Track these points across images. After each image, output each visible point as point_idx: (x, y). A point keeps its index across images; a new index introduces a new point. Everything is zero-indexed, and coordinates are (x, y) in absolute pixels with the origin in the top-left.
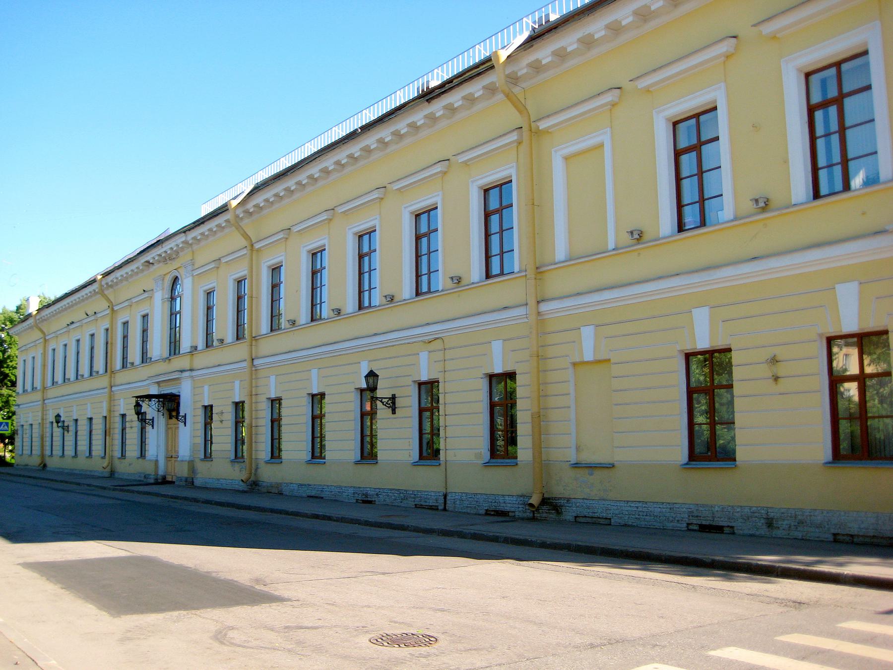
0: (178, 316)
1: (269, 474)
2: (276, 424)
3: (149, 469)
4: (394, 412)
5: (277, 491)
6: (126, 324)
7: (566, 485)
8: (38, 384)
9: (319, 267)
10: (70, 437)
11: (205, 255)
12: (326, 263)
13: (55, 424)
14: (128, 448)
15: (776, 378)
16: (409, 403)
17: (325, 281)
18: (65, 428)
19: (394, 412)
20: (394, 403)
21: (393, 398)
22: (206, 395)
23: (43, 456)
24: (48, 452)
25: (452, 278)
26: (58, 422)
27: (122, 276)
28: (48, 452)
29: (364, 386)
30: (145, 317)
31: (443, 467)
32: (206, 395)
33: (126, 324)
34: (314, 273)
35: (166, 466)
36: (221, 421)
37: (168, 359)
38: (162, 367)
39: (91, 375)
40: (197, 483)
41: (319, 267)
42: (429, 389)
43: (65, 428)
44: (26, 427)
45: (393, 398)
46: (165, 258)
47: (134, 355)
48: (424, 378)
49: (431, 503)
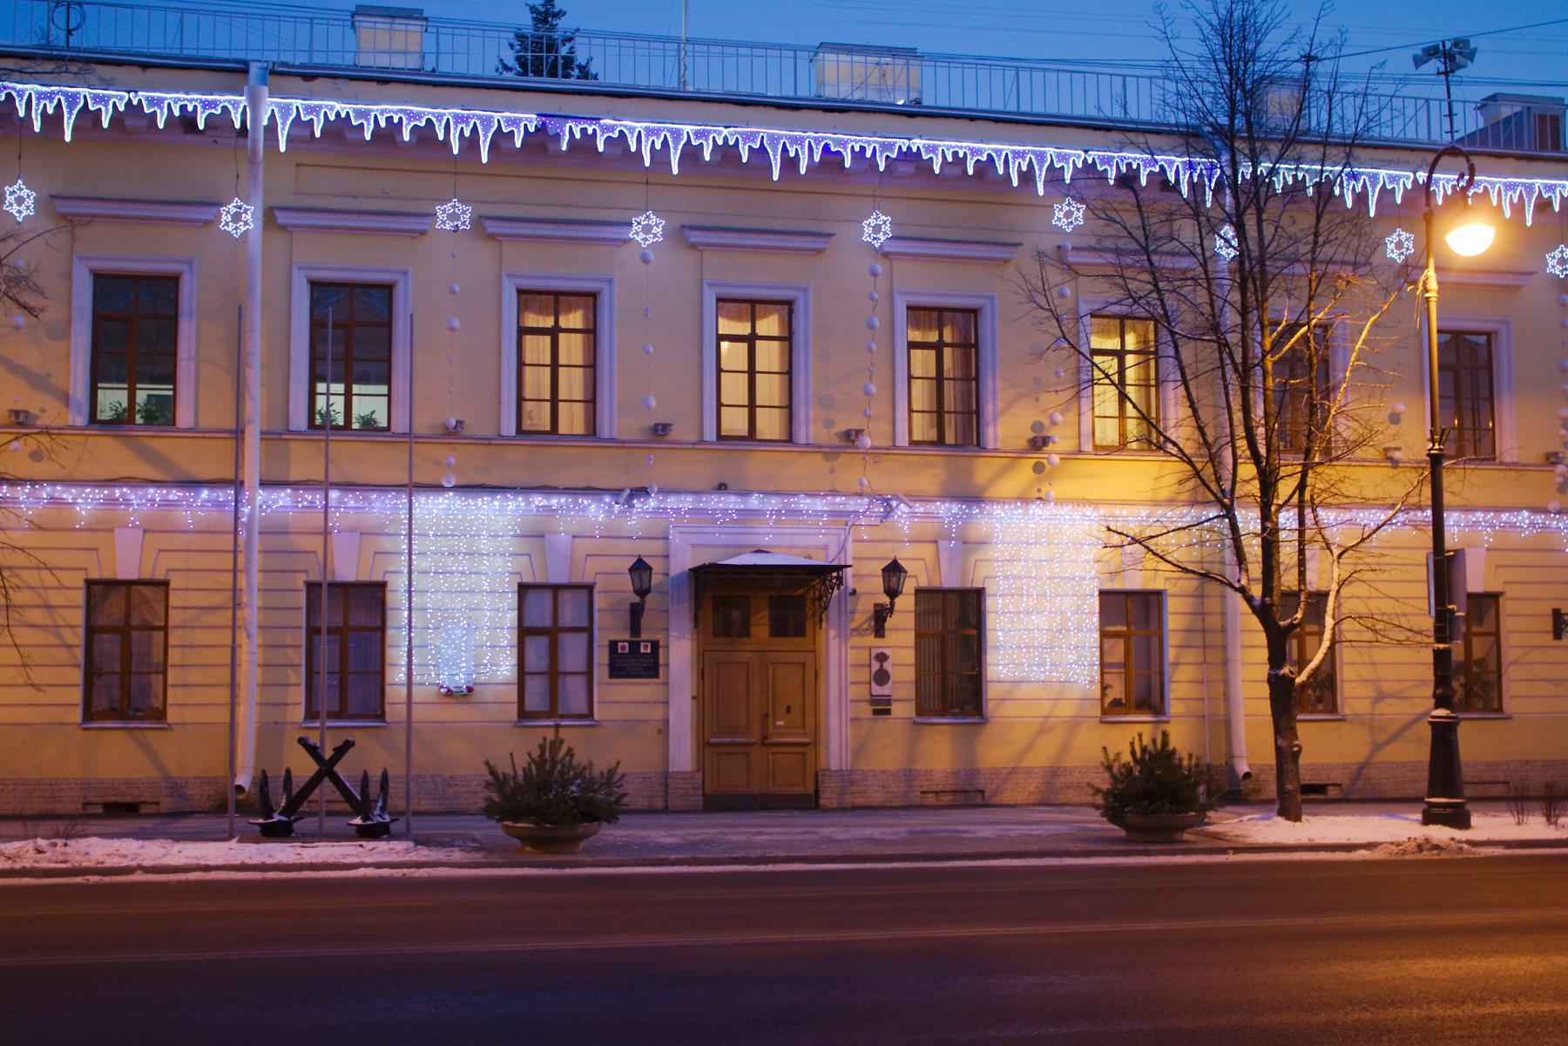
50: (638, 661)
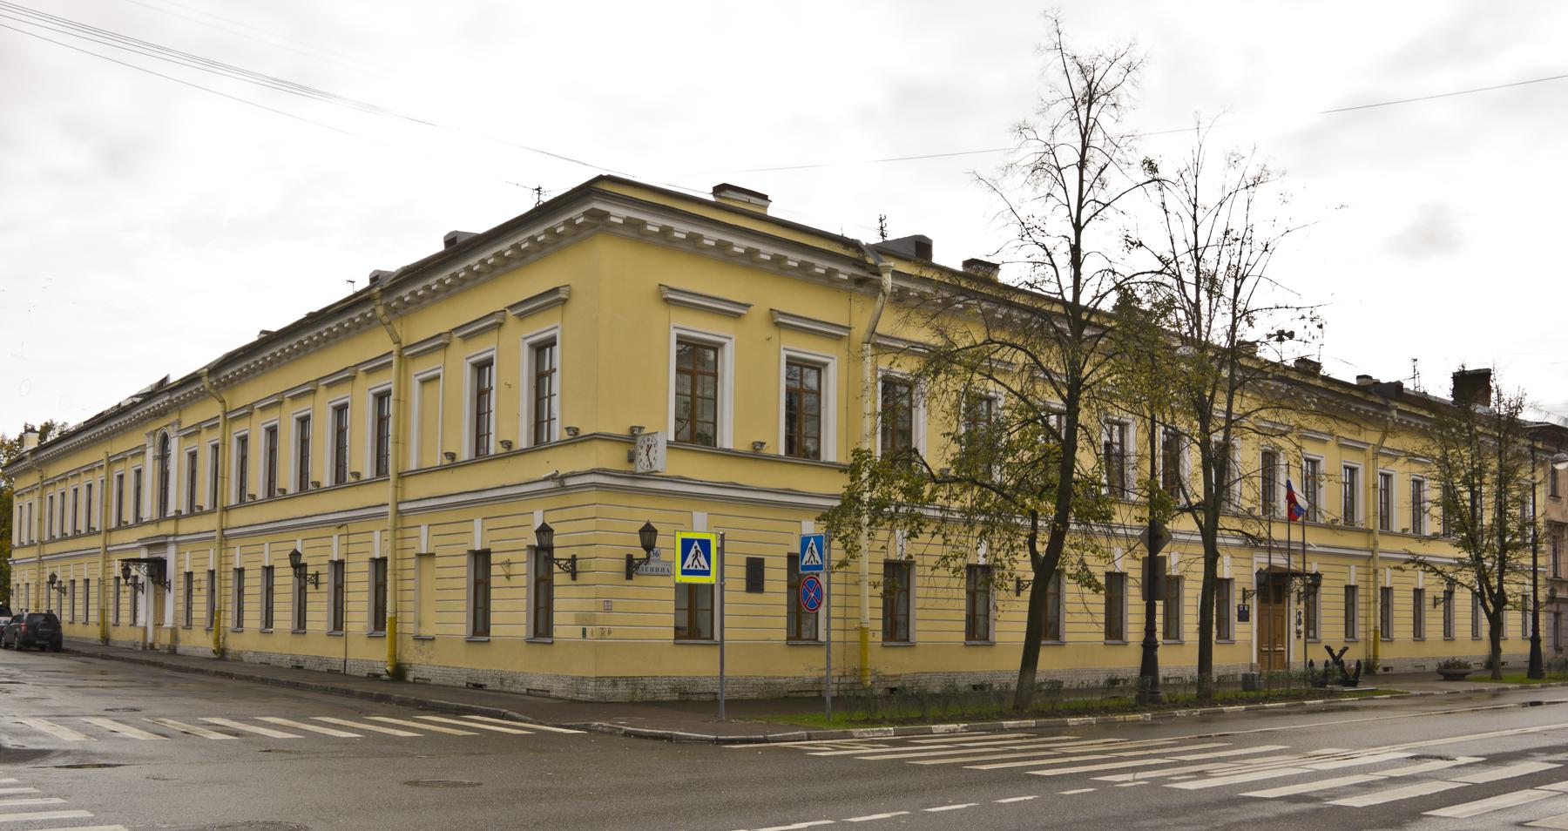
2: (481, 587)
3: (139, 637)
4: (574, 578)
6: (121, 477)
8: (96, 524)
9: (547, 368)
10: (66, 601)
11: (191, 418)
12: (557, 364)
13: (123, 581)
14: (246, 616)
15: (508, 577)
16: (326, 578)
17: (556, 389)
18: (62, 590)
19: (574, 578)
20: (574, 566)
21: (574, 559)
23: (103, 623)
24: (111, 620)
26: (126, 577)
28: (111, 620)
30: (139, 472)
33: (121, 477)
35: (155, 634)
36: (508, 577)
37: (156, 522)
38: (150, 531)
39: (192, 510)
40: (179, 650)
41: (547, 368)
42: (339, 566)
43: (62, 590)
44: (22, 587)
47: (361, 459)
48: (478, 548)
50: (1244, 616)
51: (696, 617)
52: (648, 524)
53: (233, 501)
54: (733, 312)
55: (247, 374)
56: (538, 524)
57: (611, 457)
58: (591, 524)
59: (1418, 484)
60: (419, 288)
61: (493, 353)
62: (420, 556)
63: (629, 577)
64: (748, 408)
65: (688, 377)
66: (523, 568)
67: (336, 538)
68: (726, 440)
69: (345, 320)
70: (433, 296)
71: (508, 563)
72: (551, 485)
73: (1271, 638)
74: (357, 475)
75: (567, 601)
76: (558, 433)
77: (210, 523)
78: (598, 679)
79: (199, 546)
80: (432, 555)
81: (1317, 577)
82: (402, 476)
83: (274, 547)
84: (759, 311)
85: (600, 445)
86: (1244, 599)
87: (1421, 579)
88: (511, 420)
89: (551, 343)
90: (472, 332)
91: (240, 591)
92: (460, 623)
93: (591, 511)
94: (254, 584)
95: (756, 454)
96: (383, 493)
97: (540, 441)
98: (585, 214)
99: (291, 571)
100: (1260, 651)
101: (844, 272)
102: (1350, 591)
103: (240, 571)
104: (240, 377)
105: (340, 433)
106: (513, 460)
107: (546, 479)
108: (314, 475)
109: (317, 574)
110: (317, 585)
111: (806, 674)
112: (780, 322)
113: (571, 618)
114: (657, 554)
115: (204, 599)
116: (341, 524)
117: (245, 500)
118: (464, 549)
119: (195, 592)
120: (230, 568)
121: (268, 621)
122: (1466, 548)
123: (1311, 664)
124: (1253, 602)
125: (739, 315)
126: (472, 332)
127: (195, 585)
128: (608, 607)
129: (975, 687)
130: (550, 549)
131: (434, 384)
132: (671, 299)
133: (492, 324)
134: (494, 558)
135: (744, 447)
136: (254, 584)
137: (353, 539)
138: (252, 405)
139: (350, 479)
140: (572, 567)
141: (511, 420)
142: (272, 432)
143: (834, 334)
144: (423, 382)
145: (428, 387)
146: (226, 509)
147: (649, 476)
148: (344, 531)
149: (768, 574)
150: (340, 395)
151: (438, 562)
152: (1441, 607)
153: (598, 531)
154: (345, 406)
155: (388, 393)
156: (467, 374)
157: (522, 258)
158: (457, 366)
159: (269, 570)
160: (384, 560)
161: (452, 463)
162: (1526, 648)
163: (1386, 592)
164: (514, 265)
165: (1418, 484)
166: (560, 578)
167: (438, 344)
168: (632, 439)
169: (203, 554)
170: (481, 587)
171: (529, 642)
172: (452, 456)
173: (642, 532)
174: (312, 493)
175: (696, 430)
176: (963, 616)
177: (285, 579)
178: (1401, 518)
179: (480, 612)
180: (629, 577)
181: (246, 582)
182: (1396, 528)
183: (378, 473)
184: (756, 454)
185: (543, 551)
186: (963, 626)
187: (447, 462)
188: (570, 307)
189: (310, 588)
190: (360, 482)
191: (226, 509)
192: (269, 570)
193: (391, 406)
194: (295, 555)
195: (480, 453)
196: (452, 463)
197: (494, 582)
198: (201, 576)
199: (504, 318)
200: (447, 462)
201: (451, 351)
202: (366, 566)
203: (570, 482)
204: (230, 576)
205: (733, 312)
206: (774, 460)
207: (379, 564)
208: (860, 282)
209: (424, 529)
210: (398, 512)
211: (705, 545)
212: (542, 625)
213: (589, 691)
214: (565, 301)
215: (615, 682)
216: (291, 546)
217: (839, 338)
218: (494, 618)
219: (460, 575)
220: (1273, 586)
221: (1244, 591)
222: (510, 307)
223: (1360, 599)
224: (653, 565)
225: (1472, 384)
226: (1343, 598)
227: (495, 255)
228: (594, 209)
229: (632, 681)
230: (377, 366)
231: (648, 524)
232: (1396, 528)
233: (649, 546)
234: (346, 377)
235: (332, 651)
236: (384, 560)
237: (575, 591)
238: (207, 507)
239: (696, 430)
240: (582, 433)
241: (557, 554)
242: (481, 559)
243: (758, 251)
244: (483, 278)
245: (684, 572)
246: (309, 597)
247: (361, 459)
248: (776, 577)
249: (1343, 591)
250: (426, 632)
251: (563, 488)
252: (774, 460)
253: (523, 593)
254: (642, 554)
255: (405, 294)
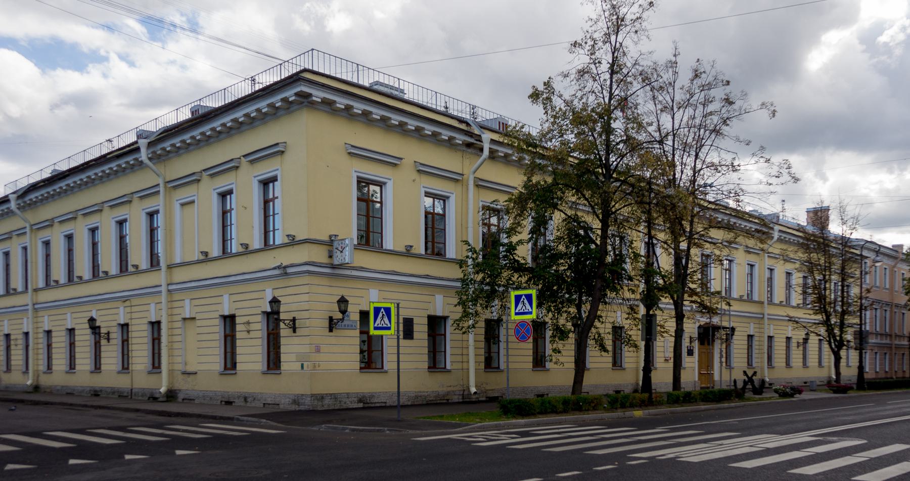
0: (271, 203)
1: (46, 381)
2: (156, 341)
4: (294, 331)
5: (51, 391)
7: (184, 385)
9: (228, 208)
15: (248, 332)
16: (116, 335)
19: (294, 331)
21: (294, 320)
22: (6, 327)
25: (288, 236)
27: (36, 197)
29: (269, 310)
31: (505, 374)
32: (6, 327)
34: (266, 202)
36: (248, 332)
41: (228, 208)
42: (125, 327)
45: (294, 320)
46: (101, 177)
47: (139, 255)
48: (227, 313)
49: (125, 394)
50: (690, 353)
51: (370, 357)
52: (343, 297)
53: (41, 284)
54: (393, 163)
55: (47, 198)
56: (270, 298)
57: (319, 255)
58: (305, 297)
59: (789, 274)
60: (177, 141)
61: (233, 186)
62: (185, 319)
63: (331, 330)
64: (401, 227)
65: (364, 204)
66: (259, 327)
67: (122, 309)
68: (388, 244)
69: (122, 162)
70: (187, 147)
71: (248, 323)
72: (277, 272)
73: (706, 364)
74: (136, 267)
75: (290, 347)
76: (280, 238)
77: (26, 299)
78: (312, 395)
79: (14, 316)
80: (194, 318)
81: (733, 329)
82: (170, 267)
83: (74, 315)
84: (408, 161)
85: (307, 246)
86: (691, 342)
87: (789, 330)
88: (247, 228)
89: (230, 192)
90: (215, 172)
91: (49, 346)
92: (216, 362)
93: (305, 289)
94: (60, 341)
95: (408, 253)
96: (160, 278)
97: (267, 246)
98: (296, 94)
99: (89, 331)
100: (700, 374)
101: (460, 138)
102: (750, 337)
103: (49, 332)
104: (42, 200)
105: (70, 251)
106: (296, 248)
107: (274, 268)
108: (54, 276)
109: (108, 333)
110: (108, 340)
111: (440, 390)
112: (423, 170)
113: (293, 357)
114: (348, 316)
115: (20, 352)
116: (125, 299)
117: (49, 283)
118: (217, 315)
119: (13, 347)
120: (41, 330)
121: (72, 366)
122: (821, 313)
123: (735, 381)
124: (696, 345)
125: (396, 165)
126: (215, 172)
127: (12, 342)
128: (318, 350)
129: (538, 396)
130: (278, 313)
131: (191, 205)
132: (356, 153)
133: (231, 167)
134: (238, 320)
135: (402, 249)
136: (60, 341)
137: (134, 309)
138: (53, 219)
139: (131, 269)
140: (293, 325)
141: (247, 228)
142: (70, 238)
143: (455, 179)
144: (182, 205)
145: (188, 209)
146: (36, 290)
147: (341, 266)
148: (128, 303)
149: (416, 328)
150: (120, 213)
151: (198, 323)
152: (801, 348)
153: (309, 301)
154: (97, 228)
155: (157, 212)
156: (215, 200)
157: (251, 122)
158: (206, 195)
159: (71, 331)
160: (159, 323)
161: (206, 258)
162: (669, 378)
163: (770, 338)
164: (257, 123)
165: (789, 274)
166: (284, 331)
167: (193, 179)
168: (330, 243)
169: (19, 321)
170: (229, 339)
171: (264, 373)
172: (206, 254)
173: (339, 302)
174: (53, 287)
175: (369, 237)
176: (531, 353)
177: (84, 337)
178: (779, 295)
179: (229, 355)
180: (331, 330)
181: (54, 340)
182: (776, 301)
183: (152, 265)
184: (408, 253)
185: (273, 316)
186: (531, 359)
187: (202, 257)
188: (287, 156)
189: (103, 342)
190: (138, 271)
191: (36, 290)
192: (71, 331)
193: (160, 220)
194: (92, 320)
195: (225, 253)
196: (206, 258)
197: (238, 335)
198: (17, 336)
199: (240, 163)
200: (202, 257)
201: (202, 184)
202: (146, 327)
203: (290, 270)
204: (41, 335)
205: (393, 163)
206: (418, 256)
207: (156, 325)
208: (469, 145)
209: (46, 317)
210: (169, 291)
211: (388, 310)
212: (274, 362)
213: (307, 404)
214: (283, 152)
215: (322, 397)
216: (89, 315)
217: (457, 180)
218: (239, 359)
219: (217, 330)
220: (707, 335)
221: (691, 338)
222: (244, 156)
223: (755, 343)
224: (345, 322)
225: (820, 216)
226: (746, 342)
227: (232, 120)
228: (299, 93)
229: (334, 396)
230: (150, 193)
231: (343, 297)
232: (776, 301)
233: (344, 312)
234: (125, 201)
235: (123, 382)
236: (159, 323)
237: (296, 340)
238: (20, 289)
239: (369, 237)
240: (297, 239)
241: (282, 316)
242: (229, 320)
243: (406, 124)
244: (223, 136)
245: (516, 314)
246: (103, 349)
247: (139, 255)
248: (421, 329)
249: (746, 338)
250: (190, 369)
251: (286, 273)
252: (418, 256)
253: (259, 342)
254: (340, 316)
255: (167, 145)
